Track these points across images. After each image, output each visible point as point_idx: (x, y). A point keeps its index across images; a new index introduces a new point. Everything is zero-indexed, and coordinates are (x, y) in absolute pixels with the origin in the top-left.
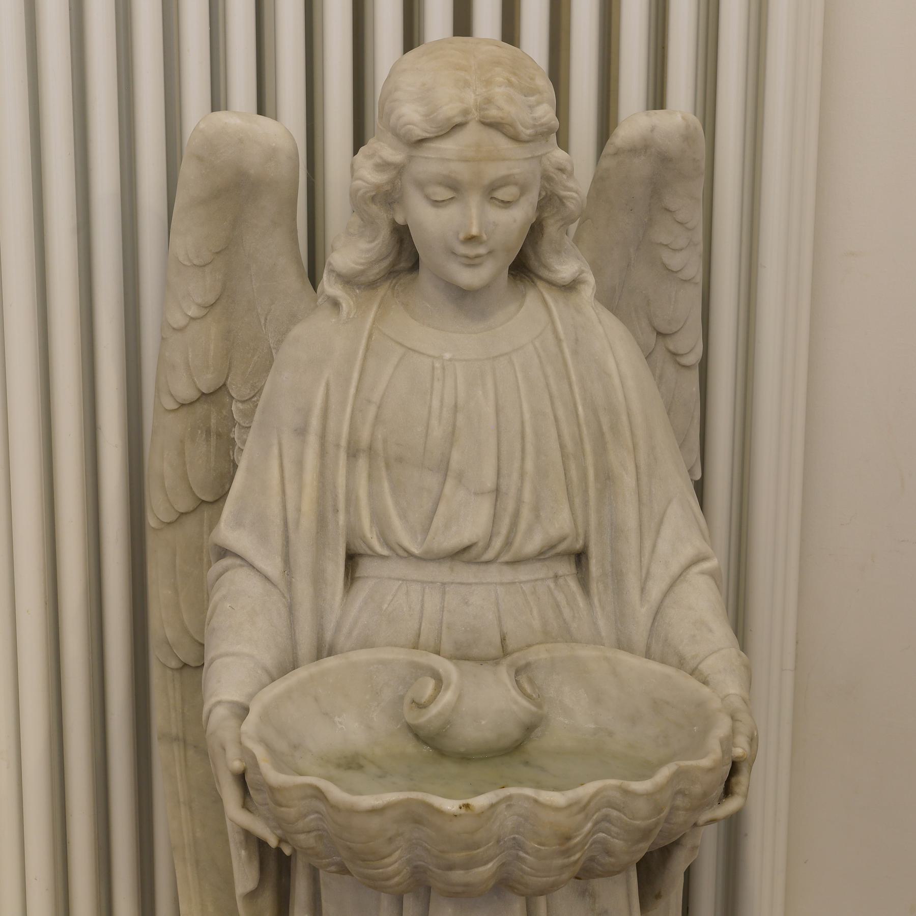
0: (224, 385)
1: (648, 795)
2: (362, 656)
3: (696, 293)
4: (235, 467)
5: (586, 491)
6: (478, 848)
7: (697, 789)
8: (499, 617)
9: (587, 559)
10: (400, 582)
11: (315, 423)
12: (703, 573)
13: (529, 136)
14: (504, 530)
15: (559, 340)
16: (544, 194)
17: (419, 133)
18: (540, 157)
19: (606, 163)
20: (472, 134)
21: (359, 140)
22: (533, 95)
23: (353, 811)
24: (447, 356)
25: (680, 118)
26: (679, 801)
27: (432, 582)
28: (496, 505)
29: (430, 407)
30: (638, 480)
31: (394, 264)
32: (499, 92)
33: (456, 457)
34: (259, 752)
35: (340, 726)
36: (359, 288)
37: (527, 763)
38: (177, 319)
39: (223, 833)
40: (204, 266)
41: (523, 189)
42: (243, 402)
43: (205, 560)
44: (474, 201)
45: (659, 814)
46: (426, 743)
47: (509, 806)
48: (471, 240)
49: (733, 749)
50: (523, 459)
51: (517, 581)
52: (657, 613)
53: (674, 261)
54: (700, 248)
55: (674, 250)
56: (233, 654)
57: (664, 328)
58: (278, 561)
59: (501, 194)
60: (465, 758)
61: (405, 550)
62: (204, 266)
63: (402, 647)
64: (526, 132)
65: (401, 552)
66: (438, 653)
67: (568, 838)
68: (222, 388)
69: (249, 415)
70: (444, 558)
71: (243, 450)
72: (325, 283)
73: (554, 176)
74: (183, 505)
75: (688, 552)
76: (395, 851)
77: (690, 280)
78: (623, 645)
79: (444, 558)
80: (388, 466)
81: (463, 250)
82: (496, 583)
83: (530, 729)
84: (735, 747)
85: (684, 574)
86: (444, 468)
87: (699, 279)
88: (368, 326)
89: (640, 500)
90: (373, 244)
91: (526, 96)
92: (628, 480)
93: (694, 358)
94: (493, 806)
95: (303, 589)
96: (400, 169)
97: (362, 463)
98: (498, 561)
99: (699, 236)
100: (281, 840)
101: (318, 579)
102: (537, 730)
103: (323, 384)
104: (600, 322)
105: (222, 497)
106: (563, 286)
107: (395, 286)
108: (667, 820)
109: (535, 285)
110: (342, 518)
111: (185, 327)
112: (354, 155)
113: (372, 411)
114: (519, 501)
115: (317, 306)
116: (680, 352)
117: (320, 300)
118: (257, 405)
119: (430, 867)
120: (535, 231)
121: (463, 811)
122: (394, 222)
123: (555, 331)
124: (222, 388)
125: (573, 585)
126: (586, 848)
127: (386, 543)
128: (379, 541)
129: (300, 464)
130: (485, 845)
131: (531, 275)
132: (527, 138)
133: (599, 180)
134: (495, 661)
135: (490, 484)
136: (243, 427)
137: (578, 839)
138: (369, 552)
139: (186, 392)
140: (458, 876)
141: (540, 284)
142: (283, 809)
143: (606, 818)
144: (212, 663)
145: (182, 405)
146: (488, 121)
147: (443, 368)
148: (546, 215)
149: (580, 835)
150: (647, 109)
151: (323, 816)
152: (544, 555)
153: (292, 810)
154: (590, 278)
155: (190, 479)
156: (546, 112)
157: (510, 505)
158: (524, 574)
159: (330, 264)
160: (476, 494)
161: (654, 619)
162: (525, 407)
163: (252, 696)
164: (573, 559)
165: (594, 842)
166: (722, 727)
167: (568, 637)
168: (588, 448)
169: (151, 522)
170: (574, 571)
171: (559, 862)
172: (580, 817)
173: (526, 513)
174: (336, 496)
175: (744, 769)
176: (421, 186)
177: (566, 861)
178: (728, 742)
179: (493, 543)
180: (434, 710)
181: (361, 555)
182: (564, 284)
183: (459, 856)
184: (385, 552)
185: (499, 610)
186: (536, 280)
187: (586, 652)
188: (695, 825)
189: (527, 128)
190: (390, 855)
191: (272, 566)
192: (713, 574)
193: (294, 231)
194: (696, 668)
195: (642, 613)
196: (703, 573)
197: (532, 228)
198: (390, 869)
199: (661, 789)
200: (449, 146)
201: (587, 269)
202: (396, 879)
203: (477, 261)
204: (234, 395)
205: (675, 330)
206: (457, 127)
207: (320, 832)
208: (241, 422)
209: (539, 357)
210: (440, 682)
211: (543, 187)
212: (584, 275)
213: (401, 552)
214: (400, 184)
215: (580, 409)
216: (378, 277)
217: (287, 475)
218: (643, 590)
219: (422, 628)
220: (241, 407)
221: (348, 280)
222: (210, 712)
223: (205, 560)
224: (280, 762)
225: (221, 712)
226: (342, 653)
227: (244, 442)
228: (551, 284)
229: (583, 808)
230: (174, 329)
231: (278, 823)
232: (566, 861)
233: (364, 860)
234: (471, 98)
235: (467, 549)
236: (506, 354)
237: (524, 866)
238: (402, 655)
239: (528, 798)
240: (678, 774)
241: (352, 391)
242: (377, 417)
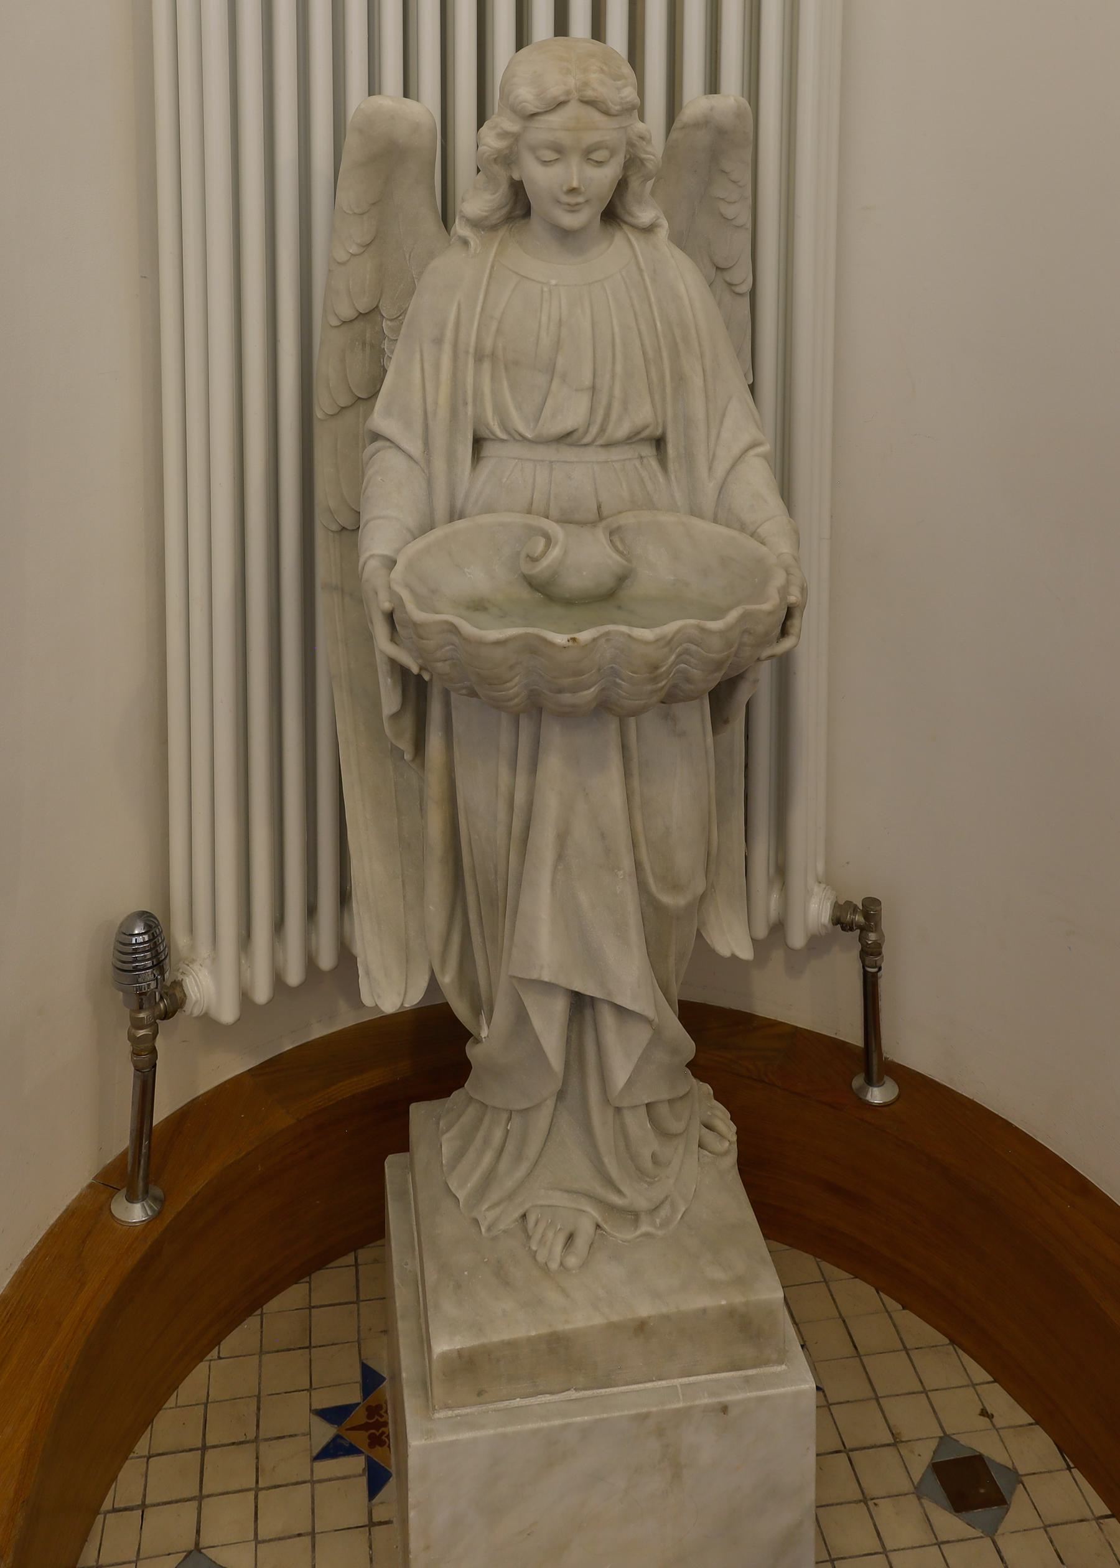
70: (551, 441)
138: (492, 437)
152: (632, 439)
181: (485, 439)
184: (504, 436)
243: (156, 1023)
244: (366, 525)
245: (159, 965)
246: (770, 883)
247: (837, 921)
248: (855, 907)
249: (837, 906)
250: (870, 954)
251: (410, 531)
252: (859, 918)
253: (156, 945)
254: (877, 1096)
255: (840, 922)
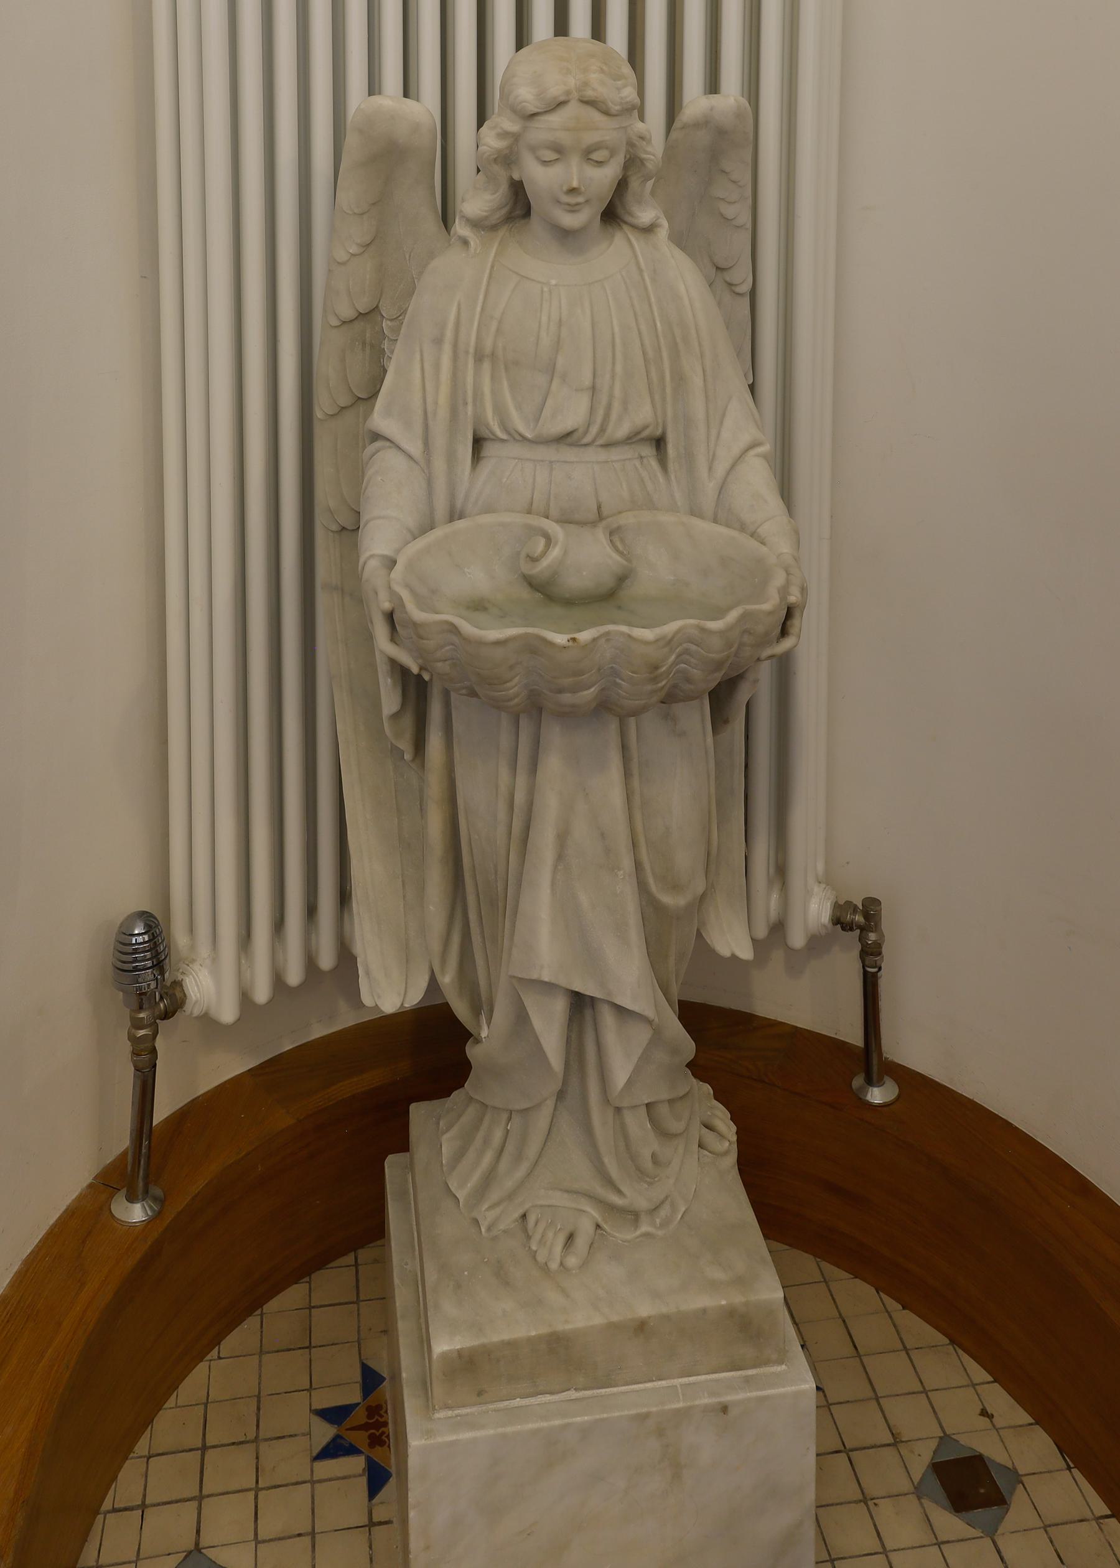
0: (377, 307)
1: (721, 633)
2: (486, 519)
3: (748, 236)
4: (385, 371)
5: (664, 389)
6: (583, 675)
7: (760, 629)
8: (596, 489)
9: (665, 444)
10: (517, 461)
11: (449, 334)
12: (758, 455)
13: (617, 111)
14: (599, 419)
15: (640, 270)
16: (628, 156)
17: (532, 109)
18: (625, 128)
19: (674, 135)
20: (573, 110)
21: (481, 119)
22: (619, 80)
23: (481, 643)
24: (553, 282)
25: (733, 100)
26: (746, 639)
27: (542, 461)
28: (592, 400)
29: (540, 322)
30: (705, 380)
31: (510, 212)
32: (594, 77)
33: (560, 361)
34: (405, 595)
35: (469, 576)
36: (483, 231)
37: (619, 608)
38: (341, 256)
39: (373, 666)
40: (362, 214)
41: (613, 153)
42: (391, 320)
43: (361, 444)
44: (575, 161)
45: (730, 648)
46: (538, 591)
47: (608, 640)
48: (572, 191)
49: (788, 597)
50: (614, 364)
51: (609, 460)
52: (722, 488)
53: (729, 211)
54: (750, 201)
55: (729, 203)
56: (383, 517)
57: (722, 265)
58: (420, 444)
59: (596, 156)
60: (570, 602)
61: (520, 435)
62: (362, 214)
63: (518, 512)
64: (615, 108)
65: (517, 437)
66: (547, 517)
67: (656, 668)
68: (376, 310)
69: (397, 330)
70: (551, 441)
71: (391, 358)
72: (457, 226)
73: (637, 143)
74: (344, 401)
75: (745, 439)
76: (515, 677)
77: (742, 226)
78: (695, 511)
79: (551, 441)
80: (506, 369)
81: (566, 199)
82: (593, 462)
83: (622, 579)
84: (789, 595)
85: (743, 456)
86: (551, 370)
87: (749, 225)
88: (491, 259)
89: (707, 397)
90: (495, 196)
91: (614, 80)
92: (697, 381)
93: (746, 287)
94: (594, 640)
95: (439, 465)
96: (516, 138)
97: (486, 366)
98: (595, 444)
99: (749, 192)
100: (421, 668)
101: (451, 458)
102: (627, 581)
103: (456, 304)
104: (673, 257)
105: (374, 395)
106: (644, 229)
107: (511, 228)
108: (736, 654)
109: (621, 228)
110: (470, 408)
111: (348, 261)
112: (516, 52)
113: (494, 326)
114: (611, 396)
115: (450, 245)
116: (734, 283)
117: (453, 240)
118: (403, 322)
119: (545, 691)
120: (622, 185)
121: (571, 643)
122: (512, 179)
123: (638, 264)
124: (376, 310)
125: (654, 464)
126: (671, 676)
127: (506, 430)
128: (500, 428)
129: (437, 366)
130: (589, 672)
131: (618, 221)
132: (614, 112)
133: (670, 151)
134: (593, 524)
135: (588, 382)
136: (392, 340)
137: (664, 668)
138: (492, 437)
139: (347, 313)
140: (567, 698)
141: (625, 227)
142: (424, 641)
143: (687, 652)
144: (367, 524)
145: (344, 322)
146: (585, 99)
147: (550, 292)
148: (630, 173)
149: (665, 665)
150: (705, 94)
151: (456, 646)
152: (632, 439)
153: (431, 642)
154: (665, 223)
155: (349, 381)
156: (629, 93)
157: (604, 400)
158: (615, 454)
159: (461, 211)
160: (576, 390)
161: (720, 492)
162: (615, 322)
163: (398, 551)
164: (654, 443)
165: (678, 672)
166: (779, 579)
167: (651, 505)
168: (665, 354)
169: (318, 414)
170: (654, 452)
171: (649, 687)
172: (666, 650)
173: (617, 406)
174: (466, 392)
175: (797, 614)
176: (533, 149)
177: (654, 687)
178: (784, 591)
179: (591, 429)
180: (545, 563)
181: (485, 439)
182: (645, 227)
183: (567, 681)
184: (504, 436)
185: (595, 484)
186: (622, 224)
187: (666, 518)
188: (759, 659)
189: (615, 105)
190: (511, 680)
191: (415, 448)
192: (764, 456)
193: (433, 187)
194: (755, 532)
195: (709, 488)
196: (758, 455)
197: (619, 184)
198: (511, 691)
199: (731, 628)
200: (555, 119)
201: (662, 216)
202: (516, 701)
203: (576, 208)
204: (385, 315)
205: (730, 265)
206: (561, 104)
207: (454, 661)
208: (390, 336)
209: (625, 283)
210: (549, 540)
211: (627, 151)
212: (660, 220)
213: (517, 437)
214: (516, 149)
215: (659, 324)
216: (498, 222)
217: (427, 375)
218: (710, 469)
219: (534, 497)
220: (390, 324)
221: (476, 224)
222: (365, 563)
223: (361, 444)
224: (422, 603)
225: (373, 564)
226: (470, 517)
227: (392, 352)
228: (634, 227)
229: (668, 642)
230: (338, 263)
231: (419, 653)
232: (654, 687)
233: (490, 684)
234: (572, 82)
235: (569, 434)
236: (600, 281)
237: (620, 691)
238: (519, 519)
239: (623, 634)
240: (745, 616)
241: (479, 309)
242: (498, 330)
243: (156, 1023)
244: (366, 525)
245: (159, 965)
246: (770, 883)
247: (837, 921)
248: (855, 907)
249: (837, 906)
250: (870, 954)
251: (410, 531)
252: (859, 918)
253: (156, 945)
254: (877, 1096)
255: (840, 922)
